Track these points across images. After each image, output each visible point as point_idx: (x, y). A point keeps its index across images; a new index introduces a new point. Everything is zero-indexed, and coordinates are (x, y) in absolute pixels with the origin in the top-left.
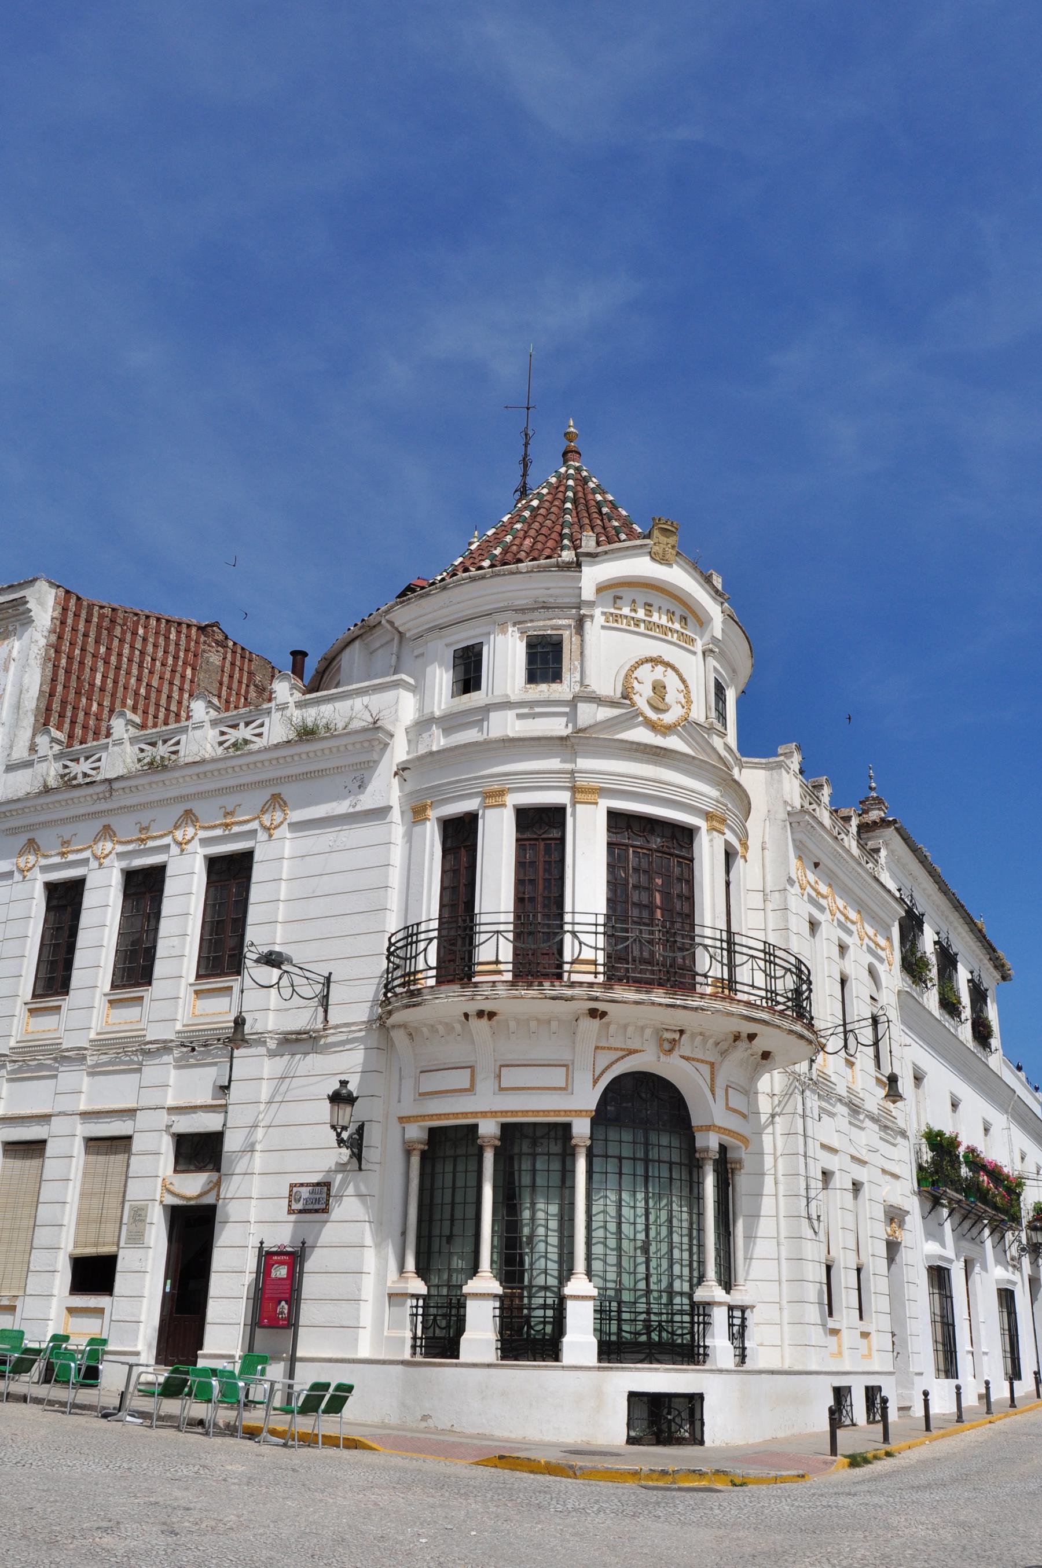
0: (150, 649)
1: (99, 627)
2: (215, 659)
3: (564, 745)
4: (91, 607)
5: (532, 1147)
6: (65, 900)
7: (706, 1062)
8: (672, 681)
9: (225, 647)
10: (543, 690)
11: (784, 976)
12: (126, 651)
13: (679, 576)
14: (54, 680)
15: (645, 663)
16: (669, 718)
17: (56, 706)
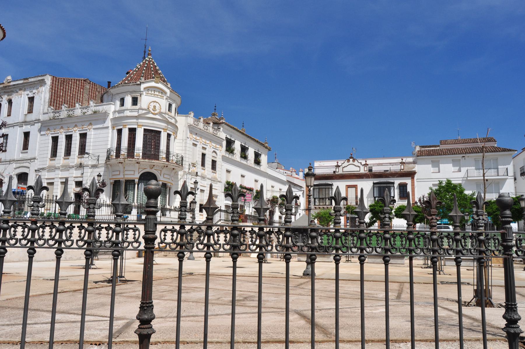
0: (73, 86)
1: (61, 83)
2: (88, 87)
3: (136, 117)
4: (59, 79)
5: (130, 183)
6: (55, 140)
8: (157, 105)
9: (90, 83)
10: (135, 107)
12: (67, 87)
13: (160, 85)
14: (52, 95)
15: (154, 100)
16: (156, 112)
17: (53, 101)
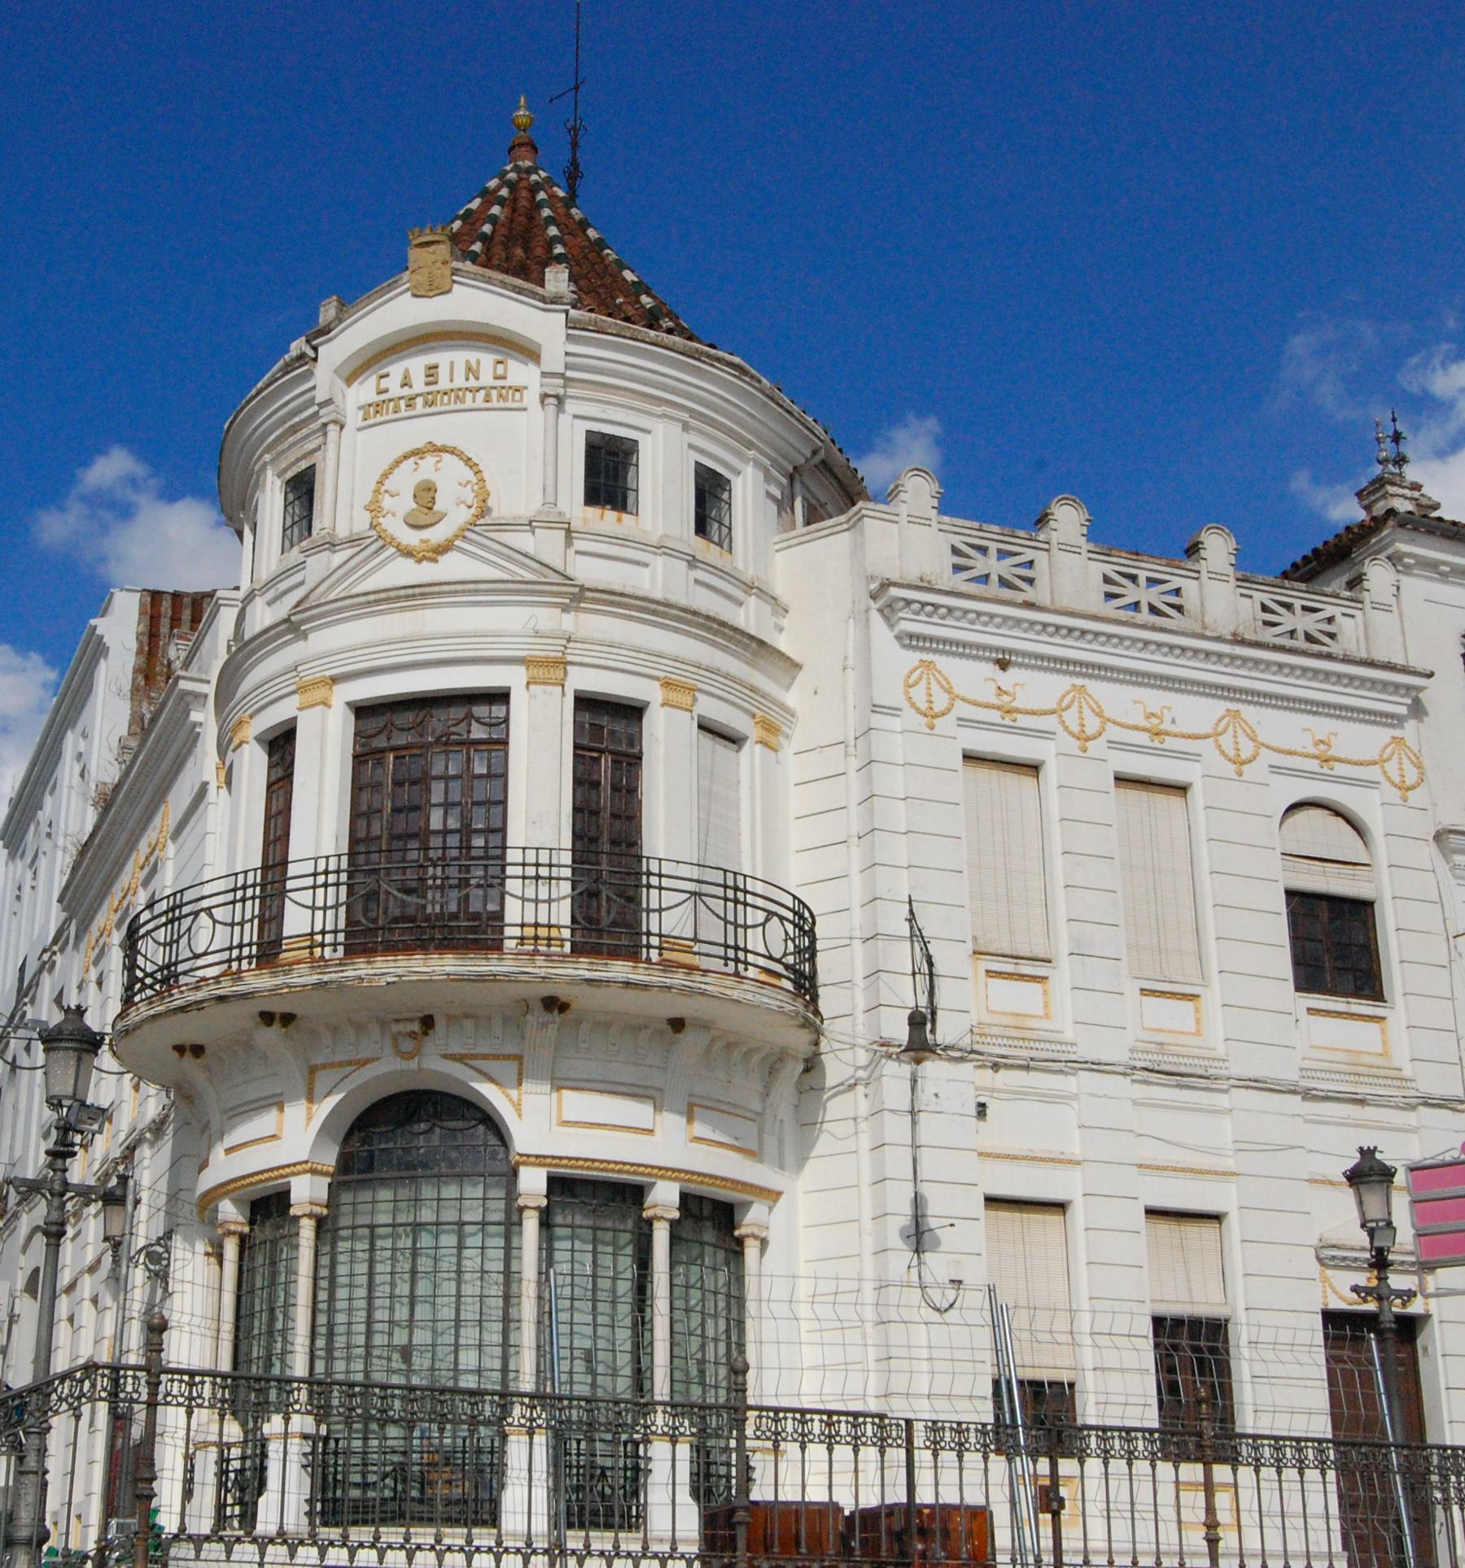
7: (507, 1057)
11: (763, 925)
